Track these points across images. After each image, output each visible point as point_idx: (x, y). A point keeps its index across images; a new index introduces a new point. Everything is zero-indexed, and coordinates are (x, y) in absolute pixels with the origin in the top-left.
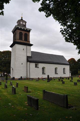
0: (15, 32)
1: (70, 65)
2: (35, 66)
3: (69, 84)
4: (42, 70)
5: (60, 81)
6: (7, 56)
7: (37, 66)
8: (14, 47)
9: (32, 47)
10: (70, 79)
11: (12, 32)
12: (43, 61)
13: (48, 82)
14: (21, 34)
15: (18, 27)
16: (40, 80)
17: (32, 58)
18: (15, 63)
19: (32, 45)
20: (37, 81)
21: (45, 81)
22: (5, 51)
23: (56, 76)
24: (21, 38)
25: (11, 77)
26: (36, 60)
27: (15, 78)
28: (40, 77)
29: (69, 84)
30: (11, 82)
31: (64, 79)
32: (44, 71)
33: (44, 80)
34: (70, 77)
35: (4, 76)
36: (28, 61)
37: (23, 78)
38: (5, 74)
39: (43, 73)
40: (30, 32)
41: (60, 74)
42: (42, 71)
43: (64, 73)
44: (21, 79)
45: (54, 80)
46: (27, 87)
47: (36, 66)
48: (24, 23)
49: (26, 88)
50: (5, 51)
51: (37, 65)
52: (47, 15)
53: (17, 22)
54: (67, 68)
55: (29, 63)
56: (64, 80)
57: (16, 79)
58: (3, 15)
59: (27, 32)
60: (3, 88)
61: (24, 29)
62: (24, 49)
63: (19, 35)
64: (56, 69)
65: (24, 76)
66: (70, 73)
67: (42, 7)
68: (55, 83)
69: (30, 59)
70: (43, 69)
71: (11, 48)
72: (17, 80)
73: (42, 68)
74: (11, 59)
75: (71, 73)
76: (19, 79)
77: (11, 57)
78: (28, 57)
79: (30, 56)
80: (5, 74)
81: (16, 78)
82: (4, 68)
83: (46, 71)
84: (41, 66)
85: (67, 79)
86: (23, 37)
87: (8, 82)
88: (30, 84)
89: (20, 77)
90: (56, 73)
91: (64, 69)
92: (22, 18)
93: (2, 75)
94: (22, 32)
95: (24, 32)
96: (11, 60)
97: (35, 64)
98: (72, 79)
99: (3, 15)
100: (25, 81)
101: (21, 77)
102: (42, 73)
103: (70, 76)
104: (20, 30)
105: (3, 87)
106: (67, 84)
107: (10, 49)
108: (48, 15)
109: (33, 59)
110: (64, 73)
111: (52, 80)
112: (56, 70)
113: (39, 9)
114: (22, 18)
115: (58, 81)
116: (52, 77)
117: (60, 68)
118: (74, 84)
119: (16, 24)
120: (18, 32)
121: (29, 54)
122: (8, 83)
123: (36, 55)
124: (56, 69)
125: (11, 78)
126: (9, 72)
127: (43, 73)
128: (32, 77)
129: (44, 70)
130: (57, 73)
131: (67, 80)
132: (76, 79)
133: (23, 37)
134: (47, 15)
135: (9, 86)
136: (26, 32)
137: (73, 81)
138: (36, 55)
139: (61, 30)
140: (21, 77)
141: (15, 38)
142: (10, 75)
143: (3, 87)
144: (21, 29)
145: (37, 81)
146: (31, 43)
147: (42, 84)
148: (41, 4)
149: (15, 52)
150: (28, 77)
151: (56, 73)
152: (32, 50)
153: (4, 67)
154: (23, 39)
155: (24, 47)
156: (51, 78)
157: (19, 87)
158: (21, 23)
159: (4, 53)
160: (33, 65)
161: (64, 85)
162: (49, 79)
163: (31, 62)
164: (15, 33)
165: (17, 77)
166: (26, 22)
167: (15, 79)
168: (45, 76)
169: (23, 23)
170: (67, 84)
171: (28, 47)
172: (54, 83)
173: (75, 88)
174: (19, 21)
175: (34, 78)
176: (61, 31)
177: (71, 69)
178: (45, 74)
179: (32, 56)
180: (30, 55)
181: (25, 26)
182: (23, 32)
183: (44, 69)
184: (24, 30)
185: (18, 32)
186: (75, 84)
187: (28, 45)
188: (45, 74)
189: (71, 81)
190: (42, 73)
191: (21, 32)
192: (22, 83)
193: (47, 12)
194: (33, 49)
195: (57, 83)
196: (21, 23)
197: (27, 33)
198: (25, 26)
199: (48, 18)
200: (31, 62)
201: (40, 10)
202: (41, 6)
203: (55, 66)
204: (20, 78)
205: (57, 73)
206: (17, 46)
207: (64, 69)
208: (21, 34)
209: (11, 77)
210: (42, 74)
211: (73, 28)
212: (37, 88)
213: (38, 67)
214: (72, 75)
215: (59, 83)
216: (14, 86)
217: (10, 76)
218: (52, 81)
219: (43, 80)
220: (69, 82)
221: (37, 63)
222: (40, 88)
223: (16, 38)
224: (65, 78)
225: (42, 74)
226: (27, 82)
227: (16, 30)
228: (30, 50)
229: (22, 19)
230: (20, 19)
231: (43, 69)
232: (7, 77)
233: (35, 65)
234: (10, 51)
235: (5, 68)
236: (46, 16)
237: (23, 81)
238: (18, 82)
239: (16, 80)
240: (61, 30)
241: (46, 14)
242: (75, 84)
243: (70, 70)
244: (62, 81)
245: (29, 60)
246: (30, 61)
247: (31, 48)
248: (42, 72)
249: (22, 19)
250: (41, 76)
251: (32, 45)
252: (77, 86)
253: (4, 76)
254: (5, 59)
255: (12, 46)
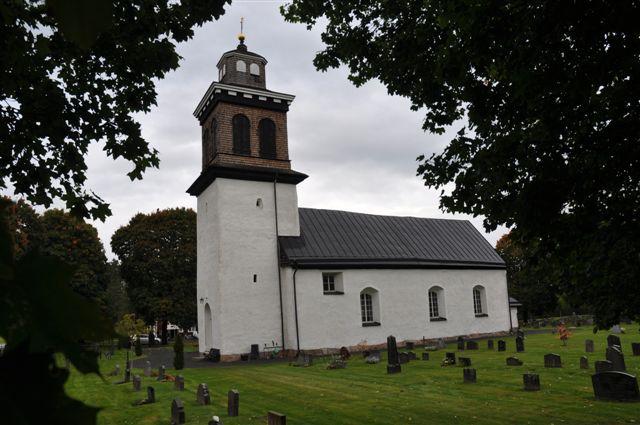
0: (209, 114)
2: (325, 288)
3: (500, 383)
4: (363, 303)
5: (454, 363)
6: (174, 236)
7: (332, 287)
8: (210, 192)
9: (300, 186)
10: (511, 344)
11: (196, 114)
12: (362, 260)
14: (241, 124)
15: (225, 92)
16: (352, 360)
18: (220, 274)
20: (335, 367)
21: (372, 367)
22: (161, 210)
23: (437, 331)
24: (241, 146)
25: (203, 348)
26: (327, 254)
28: (351, 342)
29: (500, 383)
30: (201, 386)
31: (483, 344)
32: (370, 308)
33: (375, 359)
35: (164, 343)
37: (261, 350)
39: (369, 320)
41: (460, 323)
42: (363, 308)
43: (480, 313)
44: (254, 356)
45: (426, 356)
47: (330, 287)
48: (255, 69)
50: (166, 212)
51: (332, 280)
52: (357, 74)
53: (220, 66)
55: (289, 272)
56: (474, 356)
58: (158, 167)
62: (264, 202)
63: (234, 128)
64: (434, 294)
66: (514, 312)
69: (297, 251)
70: (367, 297)
71: (195, 198)
72: (234, 363)
73: (362, 297)
75: (518, 308)
76: (244, 358)
78: (284, 243)
79: (298, 234)
80: (169, 327)
81: (225, 352)
82: (165, 302)
83: (382, 307)
84: (353, 282)
85: (496, 345)
86: (255, 140)
87: (189, 382)
89: (245, 349)
90: (436, 316)
91: (478, 291)
92: (242, 39)
93: (151, 336)
94: (249, 113)
95: (256, 111)
96: (195, 260)
98: (520, 348)
101: (255, 347)
102: (364, 319)
103: (515, 324)
106: (488, 382)
107: (191, 203)
108: (361, 74)
109: (314, 250)
110: (480, 313)
111: (413, 357)
113: (315, 61)
114: (242, 39)
116: (416, 337)
117: (456, 286)
118: (521, 380)
119: (215, 76)
120: (226, 113)
121: (290, 226)
122: (186, 386)
123: (326, 228)
124: (434, 294)
125: (198, 353)
126: (190, 320)
127: (369, 320)
129: (369, 303)
130: (441, 315)
131: (496, 358)
133: (255, 140)
134: (357, 74)
135: (194, 405)
136: (266, 114)
137: (520, 363)
138: (326, 228)
139: (421, 167)
140: (255, 347)
142: (195, 333)
143: (163, 414)
144: (239, 100)
145: (331, 368)
146: (295, 167)
149: (216, 218)
151: (436, 316)
152: (303, 203)
153: (160, 295)
154: (255, 151)
155: (262, 190)
156: (410, 345)
158: (241, 66)
159: (156, 222)
161: (471, 388)
162: (396, 355)
164: (210, 119)
165: (231, 348)
166: (263, 63)
168: (376, 338)
170: (488, 382)
171: (282, 188)
174: (227, 61)
175: (320, 351)
176: (421, 170)
177: (514, 290)
179: (307, 234)
180: (291, 229)
181: (259, 80)
182: (254, 116)
184: (254, 103)
185: (226, 113)
186: (532, 383)
190: (361, 323)
192: (259, 386)
194: (310, 195)
195: (437, 378)
196: (241, 66)
197: (273, 116)
199: (363, 87)
200: (299, 266)
201: (323, 62)
202: (323, 47)
205: (441, 315)
206: (223, 187)
207: (478, 291)
208: (241, 125)
209: (203, 348)
210: (364, 325)
211: (471, 168)
213: (337, 289)
214: (523, 317)
215: (448, 379)
218: (413, 363)
219: (368, 362)
220: (500, 368)
221: (331, 270)
224: (486, 343)
225: (364, 325)
226: (283, 377)
229: (242, 48)
231: (367, 297)
232: (180, 352)
233: (325, 280)
234: (190, 211)
235: (164, 301)
236: (350, 78)
237: (262, 371)
238: (242, 377)
240: (423, 163)
241: (353, 71)
242: (532, 383)
245: (292, 255)
246: (295, 262)
247: (295, 192)
248: (363, 313)
249: (242, 48)
250: (357, 336)
251: (301, 177)
252: (539, 394)
253: (164, 343)
254: (168, 256)
255: (196, 189)
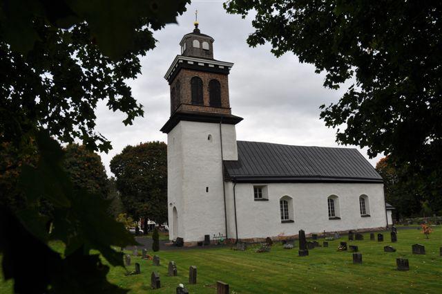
1: (385, 181)
2: (256, 196)
3: (379, 264)
4: (281, 207)
5: (346, 249)
6: (152, 161)
7: (260, 196)
8: (176, 130)
9: (238, 126)
11: (166, 78)
13: (301, 254)
14: (196, 83)
15: (185, 62)
16: (275, 246)
17: (241, 166)
19: (239, 120)
21: (291, 251)
22: (143, 143)
23: (334, 227)
24: (197, 99)
25: (172, 237)
26: (257, 172)
27: (185, 241)
30: (171, 263)
31: (367, 236)
32: (286, 210)
34: (387, 227)
35: (146, 233)
36: (227, 177)
37: (211, 239)
38: (149, 222)
39: (286, 219)
40: (229, 73)
41: (350, 221)
42: (282, 210)
43: (364, 213)
44: (206, 243)
46: (227, 287)
47: (259, 195)
48: (206, 46)
49: (224, 290)
50: (146, 144)
51: (260, 191)
52: (277, 48)
53: (182, 44)
54: (376, 194)
55: (231, 185)
56: (361, 245)
57: (190, 243)
59: (216, 75)
60: (148, 285)
61: (206, 65)
62: (213, 137)
64: (331, 201)
65: (215, 230)
66: (390, 214)
67: (257, 32)
68: (328, 261)
69: (236, 171)
70: (285, 202)
73: (281, 202)
74: (166, 171)
75: (392, 210)
76: (200, 244)
77: (166, 165)
78: (227, 165)
83: (295, 210)
84: (275, 192)
85: (376, 238)
86: (206, 94)
87: (163, 260)
88: (238, 269)
90: (333, 216)
91: (363, 199)
92: (196, 25)
93: (137, 229)
96: (166, 177)
97: (254, 186)
98: (394, 239)
99: (153, 275)
100: (219, 251)
101: (207, 237)
102: (282, 218)
103: (390, 223)
104: (191, 70)
105: (148, 283)
106: (371, 264)
107: (163, 138)
108: (280, 49)
110: (364, 213)
111: (316, 244)
112: (333, 205)
113: (248, 40)
114: (196, 25)
115: (339, 250)
116: (319, 231)
117: (347, 195)
120: (187, 76)
121: (231, 153)
122: (160, 263)
124: (331, 201)
125: (168, 240)
126: (163, 218)
127: (286, 219)
128: (243, 236)
129: (286, 207)
132: (411, 234)
133: (206, 94)
134: (277, 48)
136: (214, 76)
137: (394, 251)
140: (207, 237)
141: (176, 98)
142: (166, 226)
143: (145, 281)
144: (195, 67)
146: (234, 113)
147: (279, 267)
148: (254, 24)
149: (180, 148)
150: (233, 236)
151: (333, 216)
152: (240, 138)
153: (143, 201)
154: (207, 101)
155: (211, 129)
157: (202, 281)
158: (196, 44)
159: (140, 151)
160: (246, 191)
161: (359, 267)
163: (237, 181)
164: (176, 80)
166: (211, 41)
167: (185, 245)
168: (291, 231)
169: (201, 43)
170: (371, 264)
171: (225, 127)
172: (323, 256)
173: (402, 280)
175: (252, 239)
178: (293, 222)
179: (243, 159)
180: (232, 155)
182: (206, 78)
183: (286, 202)
184: (206, 69)
185: (187, 76)
186: (403, 265)
187: (223, 123)
188: (293, 222)
189: (387, 249)
191: (198, 78)
192: (210, 264)
193: (276, 40)
194: (243, 132)
196: (196, 44)
197: (219, 78)
198: (209, 53)
199: (282, 57)
201: (253, 41)
203: (322, 192)
204: (203, 239)
206: (185, 127)
207: (363, 199)
208: (196, 84)
209: (172, 237)
210: (283, 222)
212: (260, 283)
213: (263, 197)
214: (396, 217)
215: (342, 260)
216: (182, 285)
217: (167, 231)
218: (316, 249)
219: (285, 248)
221: (259, 183)
222: (270, 286)
223: (182, 100)
224: (368, 235)
225: (283, 222)
226: (226, 257)
227: (179, 72)
228: (234, 136)
229: (197, 31)
230: (191, 29)
231: (285, 202)
233: (255, 191)
235: (145, 205)
236: (272, 51)
239: (186, 247)
240: (324, 110)
241: (274, 46)
242: (403, 265)
243: (387, 201)
244: (355, 248)
245: (232, 173)
246: (235, 178)
247: (234, 130)
248: (282, 214)
249: (197, 31)
250: (277, 230)
251: (239, 120)
252: (408, 273)
253: (146, 233)
255: (167, 129)
